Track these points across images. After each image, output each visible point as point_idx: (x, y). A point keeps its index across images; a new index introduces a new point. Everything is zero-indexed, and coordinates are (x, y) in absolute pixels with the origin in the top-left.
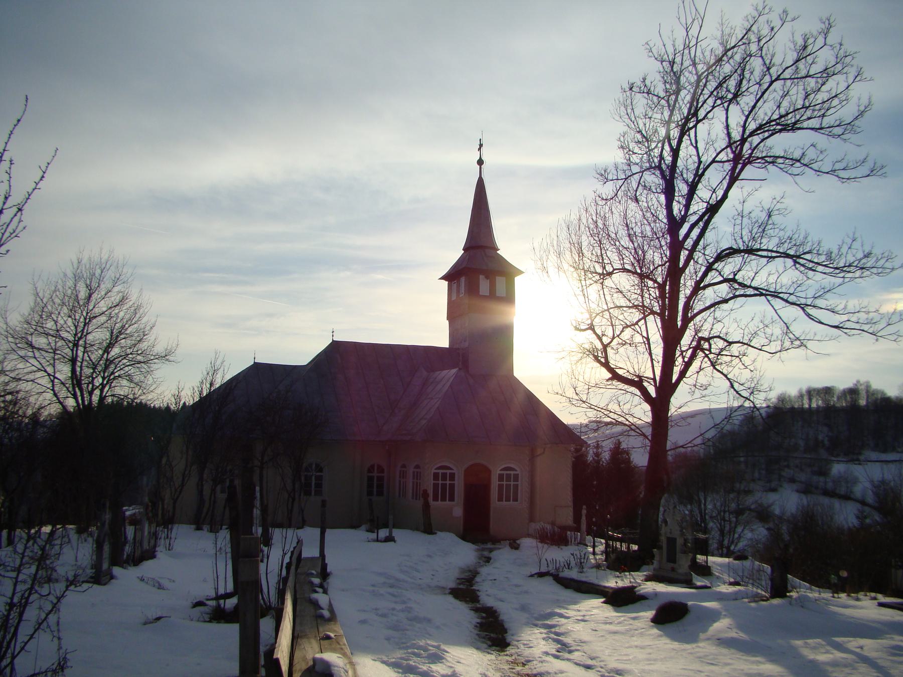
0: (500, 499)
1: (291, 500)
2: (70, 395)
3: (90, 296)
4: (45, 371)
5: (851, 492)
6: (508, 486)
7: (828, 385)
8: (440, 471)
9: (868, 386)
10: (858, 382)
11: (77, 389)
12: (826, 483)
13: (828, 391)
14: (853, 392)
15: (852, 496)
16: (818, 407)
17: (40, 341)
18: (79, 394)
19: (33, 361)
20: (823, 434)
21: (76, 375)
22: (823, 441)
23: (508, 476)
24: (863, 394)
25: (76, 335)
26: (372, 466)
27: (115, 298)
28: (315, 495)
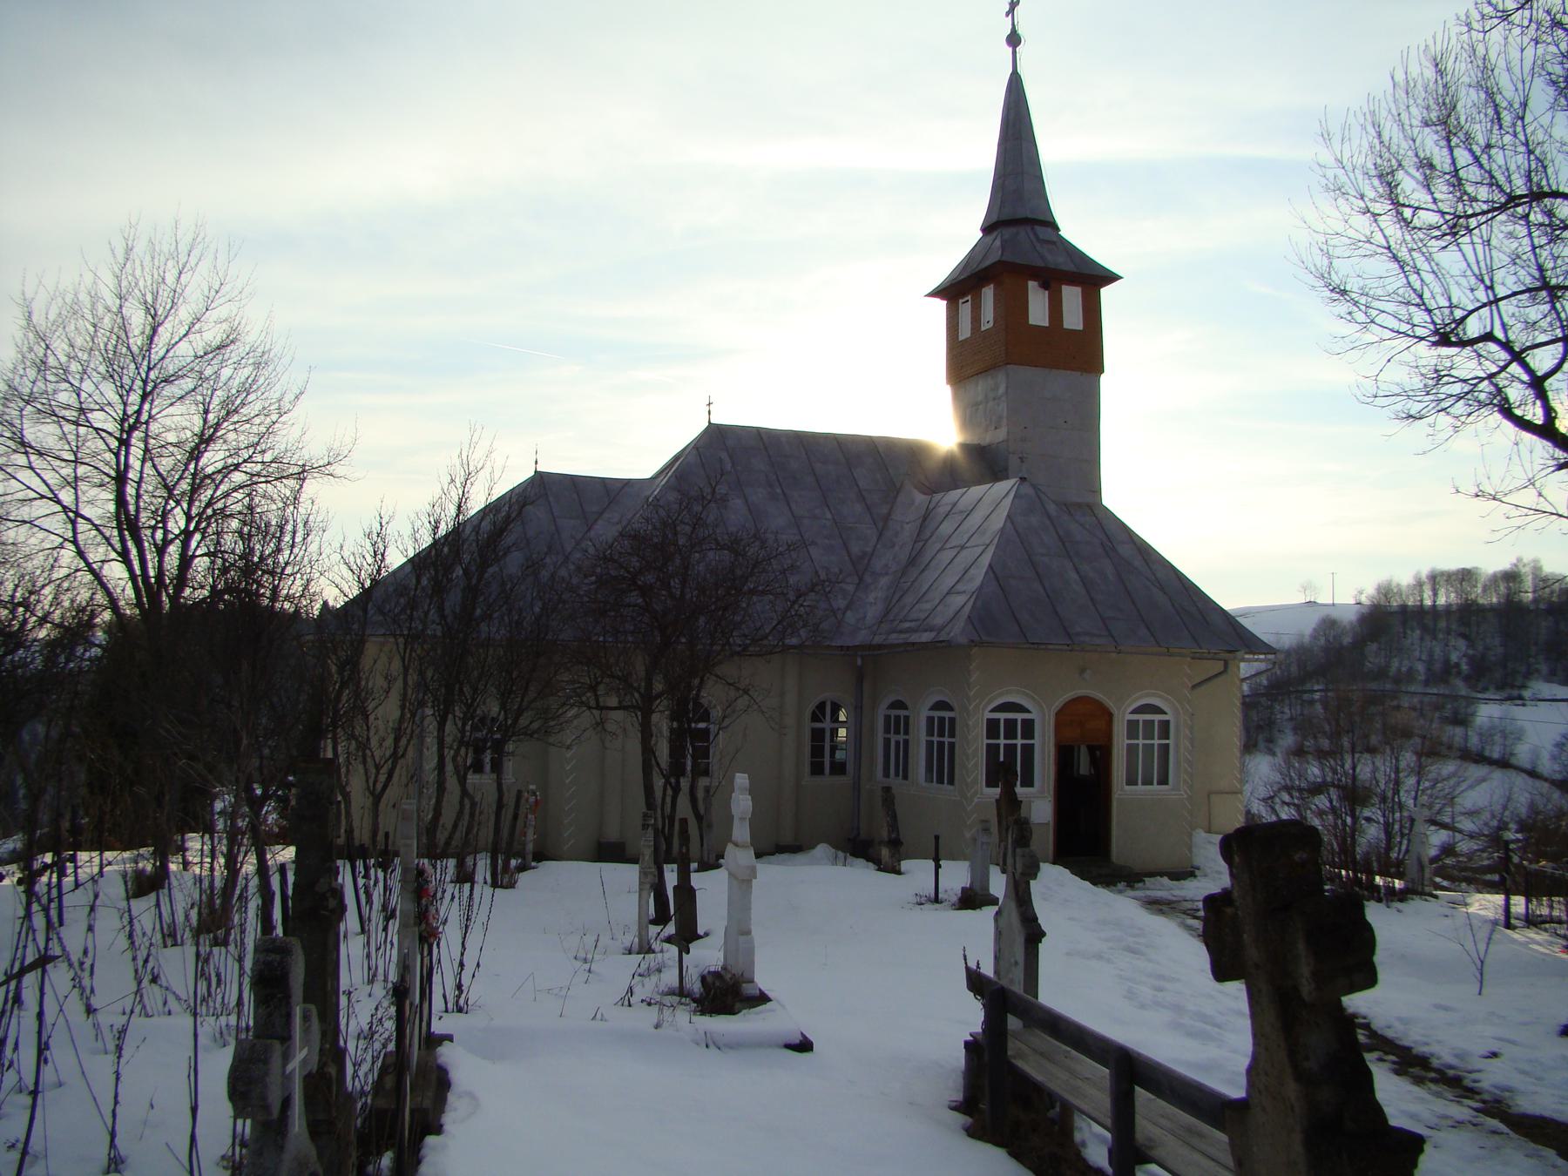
0: (1131, 781)
1: (669, 792)
2: (113, 555)
3: (154, 330)
4: (59, 502)
5: (1512, 754)
7: (1468, 566)
8: (1002, 716)
9: (1537, 569)
10: (1519, 560)
11: (130, 544)
12: (1466, 738)
13: (1466, 576)
14: (1511, 577)
15: (1514, 761)
16: (1448, 607)
17: (43, 433)
18: (134, 552)
19: (26, 476)
20: (1458, 651)
21: (127, 512)
22: (1457, 665)
23: (1010, 724)
24: (1528, 584)
25: (123, 420)
26: (821, 706)
27: (212, 334)
28: (832, 773)
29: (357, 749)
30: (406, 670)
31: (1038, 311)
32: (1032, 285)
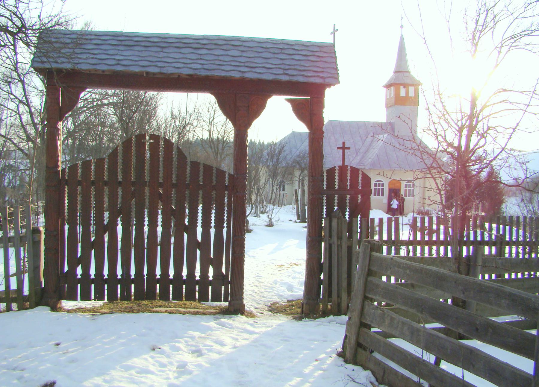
6: (409, 190)
8: (377, 183)
23: (379, 185)
29: (107, 99)
30: (266, 172)
31: (403, 93)
32: (402, 87)
